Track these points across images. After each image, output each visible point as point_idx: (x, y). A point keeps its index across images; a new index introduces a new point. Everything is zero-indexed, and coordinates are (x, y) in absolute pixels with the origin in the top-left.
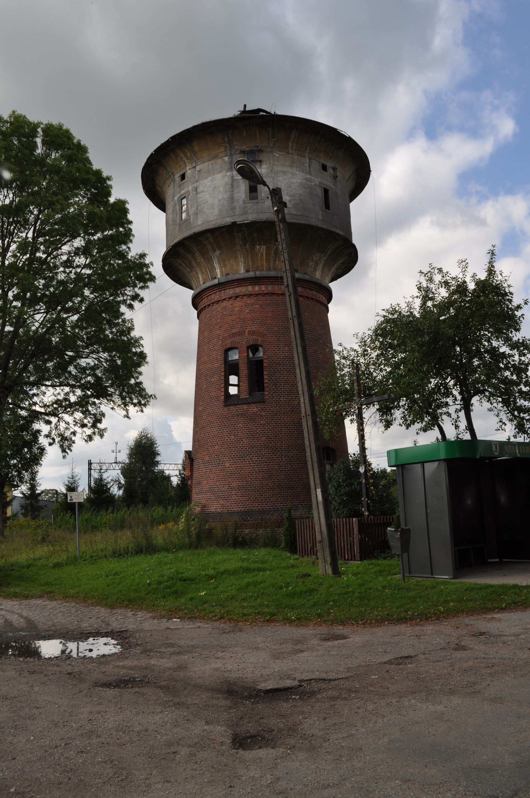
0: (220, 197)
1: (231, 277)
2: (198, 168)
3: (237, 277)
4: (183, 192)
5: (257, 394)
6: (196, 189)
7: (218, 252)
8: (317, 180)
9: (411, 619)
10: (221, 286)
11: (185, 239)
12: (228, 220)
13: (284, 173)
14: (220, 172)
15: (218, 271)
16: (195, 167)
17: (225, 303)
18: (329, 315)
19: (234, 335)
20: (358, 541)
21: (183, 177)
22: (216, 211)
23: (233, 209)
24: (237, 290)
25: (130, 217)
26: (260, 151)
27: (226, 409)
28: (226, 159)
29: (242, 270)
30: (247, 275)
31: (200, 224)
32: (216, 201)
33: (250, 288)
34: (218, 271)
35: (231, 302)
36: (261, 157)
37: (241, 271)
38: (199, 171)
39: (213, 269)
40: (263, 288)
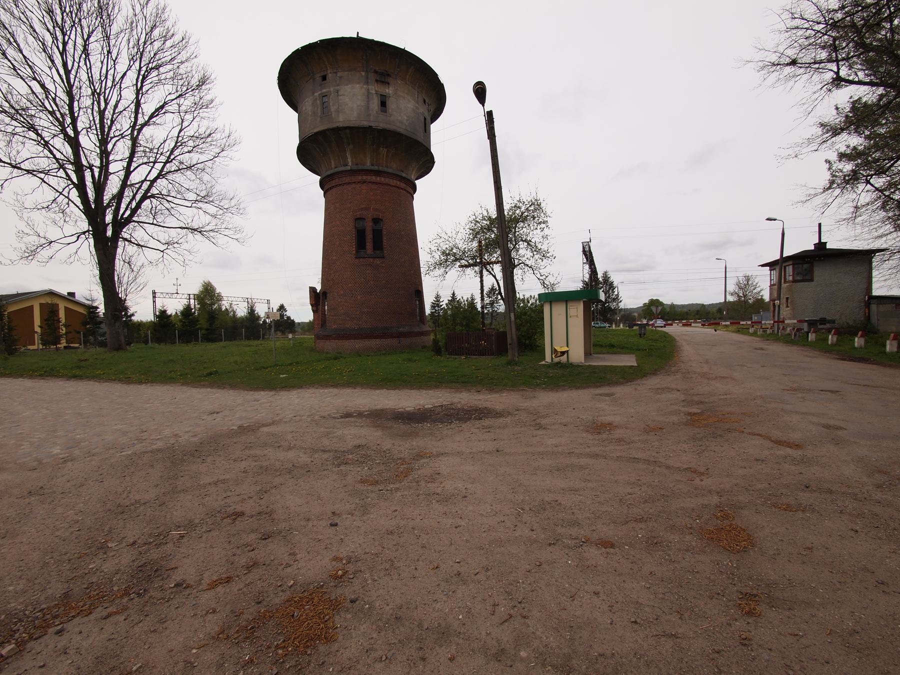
0: (359, 103)
1: (361, 167)
2: (339, 74)
3: (365, 167)
4: (324, 91)
5: (378, 252)
6: (337, 92)
7: (351, 146)
8: (421, 110)
9: (476, 410)
10: (352, 172)
11: (328, 130)
12: (365, 124)
13: (404, 98)
14: (359, 83)
15: (349, 160)
16: (336, 73)
17: (354, 186)
18: (414, 202)
19: (362, 209)
20: (488, 405)
21: (324, 78)
22: (355, 114)
23: (369, 115)
24: (364, 178)
25: (823, 99)
26: (388, 75)
27: (357, 260)
28: (363, 74)
29: (368, 163)
30: (372, 168)
31: (341, 120)
32: (355, 106)
33: (374, 178)
34: (349, 160)
35: (359, 185)
36: (390, 80)
37: (368, 165)
38: (341, 77)
39: (345, 158)
40: (383, 179)
